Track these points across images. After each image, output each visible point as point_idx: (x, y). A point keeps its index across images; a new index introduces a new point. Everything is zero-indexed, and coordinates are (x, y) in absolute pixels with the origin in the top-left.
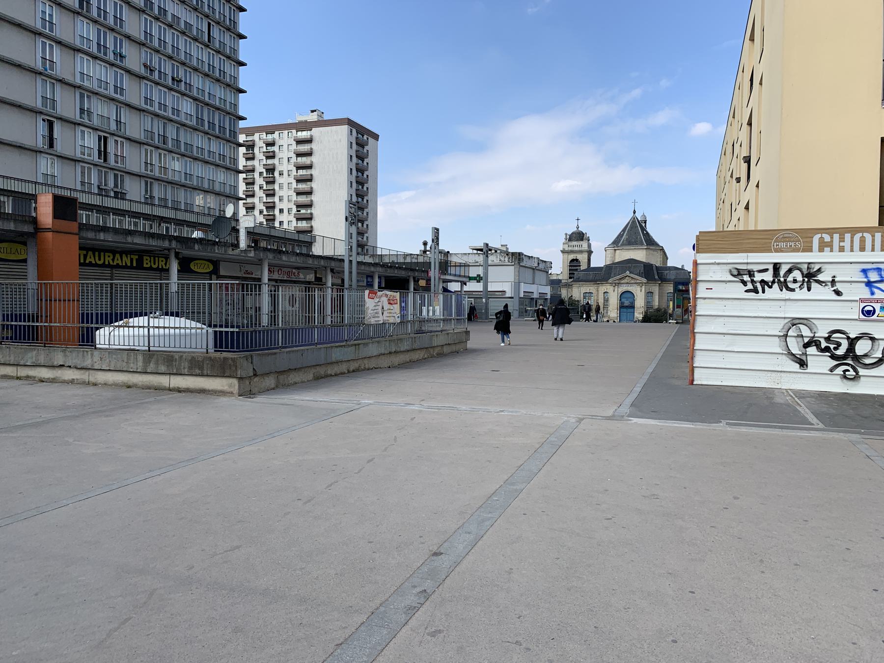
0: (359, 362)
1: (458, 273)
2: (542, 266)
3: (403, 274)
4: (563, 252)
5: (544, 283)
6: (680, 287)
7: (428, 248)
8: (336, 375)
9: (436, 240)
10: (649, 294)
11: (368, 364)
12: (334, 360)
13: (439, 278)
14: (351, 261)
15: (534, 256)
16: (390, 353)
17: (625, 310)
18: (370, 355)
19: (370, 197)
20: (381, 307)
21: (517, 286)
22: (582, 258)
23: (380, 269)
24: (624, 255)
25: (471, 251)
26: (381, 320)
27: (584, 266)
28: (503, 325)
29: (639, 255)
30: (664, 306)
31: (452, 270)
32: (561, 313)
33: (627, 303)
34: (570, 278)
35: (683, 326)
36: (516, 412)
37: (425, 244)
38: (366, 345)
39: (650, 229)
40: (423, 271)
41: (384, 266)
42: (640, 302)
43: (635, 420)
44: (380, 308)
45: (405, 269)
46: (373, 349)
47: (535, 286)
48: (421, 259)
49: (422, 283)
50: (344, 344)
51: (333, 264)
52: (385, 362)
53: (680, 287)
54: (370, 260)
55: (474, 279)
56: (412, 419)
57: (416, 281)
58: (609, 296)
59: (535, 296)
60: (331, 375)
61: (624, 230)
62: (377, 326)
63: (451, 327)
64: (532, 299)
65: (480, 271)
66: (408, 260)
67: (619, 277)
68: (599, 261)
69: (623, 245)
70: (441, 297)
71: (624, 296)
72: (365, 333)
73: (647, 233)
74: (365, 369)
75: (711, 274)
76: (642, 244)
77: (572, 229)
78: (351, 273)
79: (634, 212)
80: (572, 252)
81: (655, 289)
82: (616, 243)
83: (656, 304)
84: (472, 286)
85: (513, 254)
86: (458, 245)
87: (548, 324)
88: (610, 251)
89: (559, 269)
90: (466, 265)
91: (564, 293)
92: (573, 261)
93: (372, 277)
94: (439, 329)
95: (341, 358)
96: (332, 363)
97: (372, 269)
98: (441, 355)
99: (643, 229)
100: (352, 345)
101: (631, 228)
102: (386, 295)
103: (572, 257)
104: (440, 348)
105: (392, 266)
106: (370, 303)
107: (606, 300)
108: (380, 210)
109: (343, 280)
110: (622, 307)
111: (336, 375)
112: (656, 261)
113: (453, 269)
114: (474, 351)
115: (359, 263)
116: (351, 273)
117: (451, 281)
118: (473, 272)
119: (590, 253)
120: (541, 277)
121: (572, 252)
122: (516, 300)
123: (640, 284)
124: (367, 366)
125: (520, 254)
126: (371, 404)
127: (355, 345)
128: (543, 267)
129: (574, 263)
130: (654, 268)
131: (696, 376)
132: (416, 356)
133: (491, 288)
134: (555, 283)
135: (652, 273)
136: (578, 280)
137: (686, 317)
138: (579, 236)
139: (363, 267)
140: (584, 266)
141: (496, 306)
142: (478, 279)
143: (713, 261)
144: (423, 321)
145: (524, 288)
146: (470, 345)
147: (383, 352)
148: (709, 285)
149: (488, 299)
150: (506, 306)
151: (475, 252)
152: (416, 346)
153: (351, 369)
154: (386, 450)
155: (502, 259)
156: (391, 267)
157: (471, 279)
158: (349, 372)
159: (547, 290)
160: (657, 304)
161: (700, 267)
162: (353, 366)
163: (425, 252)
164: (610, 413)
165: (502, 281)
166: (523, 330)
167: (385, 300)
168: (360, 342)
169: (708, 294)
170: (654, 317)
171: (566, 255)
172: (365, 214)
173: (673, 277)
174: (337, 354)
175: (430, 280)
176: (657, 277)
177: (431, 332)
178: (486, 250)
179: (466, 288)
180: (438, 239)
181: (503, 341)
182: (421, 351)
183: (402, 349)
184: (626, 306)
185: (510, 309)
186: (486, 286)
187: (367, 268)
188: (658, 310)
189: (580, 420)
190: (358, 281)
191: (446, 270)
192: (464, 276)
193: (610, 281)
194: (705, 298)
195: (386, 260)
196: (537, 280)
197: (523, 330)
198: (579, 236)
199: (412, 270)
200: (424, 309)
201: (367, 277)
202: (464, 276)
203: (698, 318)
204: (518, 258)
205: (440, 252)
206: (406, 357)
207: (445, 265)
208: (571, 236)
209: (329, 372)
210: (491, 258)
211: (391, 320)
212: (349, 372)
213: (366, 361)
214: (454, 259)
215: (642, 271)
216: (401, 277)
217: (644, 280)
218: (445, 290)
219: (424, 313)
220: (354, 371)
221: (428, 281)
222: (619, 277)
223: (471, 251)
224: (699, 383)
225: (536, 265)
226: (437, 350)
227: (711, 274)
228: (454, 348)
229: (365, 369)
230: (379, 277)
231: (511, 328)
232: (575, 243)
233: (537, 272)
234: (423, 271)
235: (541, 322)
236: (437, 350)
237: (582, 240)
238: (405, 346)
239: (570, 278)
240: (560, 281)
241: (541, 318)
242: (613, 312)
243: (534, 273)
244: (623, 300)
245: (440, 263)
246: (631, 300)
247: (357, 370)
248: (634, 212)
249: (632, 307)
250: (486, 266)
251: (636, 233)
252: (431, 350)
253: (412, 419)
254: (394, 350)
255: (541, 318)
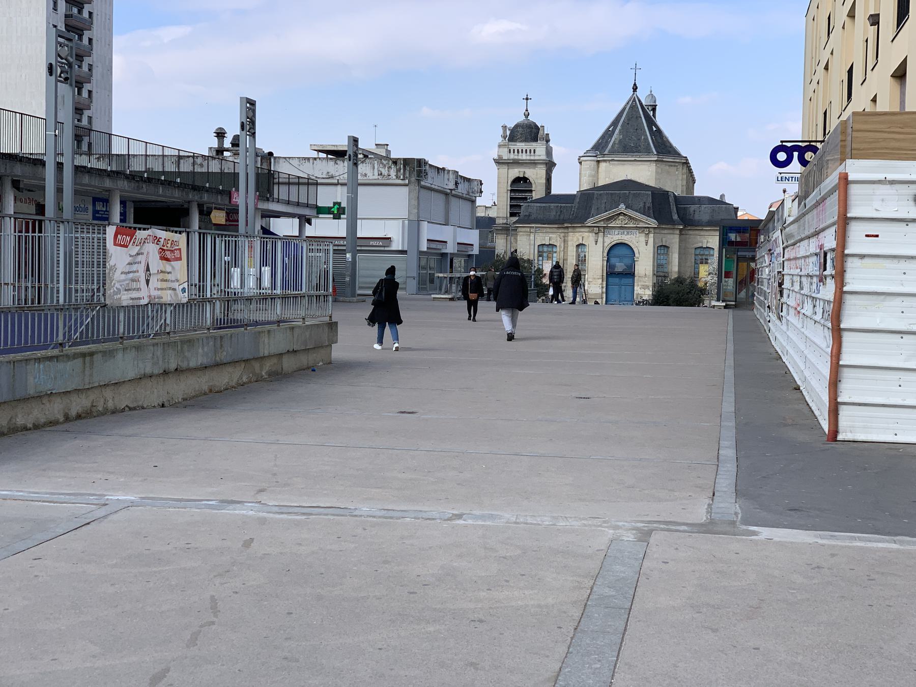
0: (92, 396)
1: (294, 198)
2: (462, 189)
3: (175, 196)
4: (499, 162)
5: (468, 224)
6: (732, 236)
7: (227, 144)
8: (36, 427)
9: (249, 125)
10: (662, 249)
11: (113, 399)
12: (32, 392)
13: (256, 209)
14: (60, 166)
15: (449, 167)
16: (166, 373)
17: (616, 280)
18: (117, 376)
19: (95, 32)
20: (144, 269)
21: (414, 227)
22: (536, 175)
23: (123, 184)
24: (616, 171)
25: (315, 154)
26: (144, 295)
27: (538, 193)
28: (385, 310)
29: (643, 172)
30: (688, 274)
31: (281, 192)
32: (510, 286)
33: (620, 267)
34: (512, 215)
35: (739, 313)
36: (492, 517)
37: (220, 134)
38: (109, 354)
39: (662, 120)
40: (221, 192)
41: (134, 177)
42: (644, 266)
43: (765, 532)
44: (142, 268)
45: (181, 186)
46: (125, 365)
47: (449, 229)
48: (214, 167)
49: (218, 217)
50: (50, 352)
51: (18, 170)
52: (153, 393)
53: (732, 236)
54: (102, 165)
55: (328, 210)
56: (248, 543)
57: (205, 213)
58: (587, 249)
59: (450, 249)
60: (25, 429)
61: (615, 123)
62: (136, 311)
63: (296, 313)
64: (444, 255)
65: (340, 195)
66: (186, 167)
67: (605, 215)
68: (567, 182)
69: (612, 152)
70: (257, 244)
71: (616, 251)
72: (101, 325)
73: (659, 131)
74: (105, 412)
75: (877, 204)
76: (648, 151)
77: (515, 118)
78: (59, 191)
79: (635, 88)
80: (516, 163)
81: (673, 240)
82: (599, 147)
83: (674, 268)
84: (323, 227)
85: (407, 162)
86: (288, 139)
87: (486, 307)
88: (589, 164)
89: (492, 198)
90: (311, 183)
91: (501, 246)
92: (517, 180)
93: (106, 201)
94: (274, 318)
95: (48, 387)
96: (26, 399)
97: (108, 183)
98: (278, 376)
99: (651, 122)
100: (76, 356)
101: (629, 118)
102: (157, 240)
103: (515, 172)
104: (275, 360)
105: (151, 179)
106: (118, 258)
107: (581, 260)
108: (118, 62)
109: (41, 209)
110: (611, 274)
111: (36, 427)
112: (674, 185)
113: (284, 189)
114: (346, 367)
115: (78, 170)
116: (59, 191)
117: (278, 215)
118: (325, 197)
119: (550, 165)
120: (459, 208)
121: (516, 163)
122: (413, 256)
123: (646, 230)
124: (110, 405)
125: (421, 162)
126: (133, 504)
127: (83, 355)
128: (464, 190)
129: (520, 186)
130: (671, 199)
131: (843, 422)
132: (223, 378)
133: (365, 230)
134: (485, 225)
135: (672, 210)
136: (528, 220)
137: (743, 294)
138: (529, 132)
139: (86, 179)
140: (538, 193)
141: (371, 271)
142: (337, 212)
143: (881, 177)
144: (230, 300)
145: (428, 232)
146: (338, 352)
147: (148, 370)
148: (872, 228)
149: (355, 253)
150: (391, 271)
151: (324, 155)
152: (223, 356)
153: (73, 413)
154: (193, 641)
155: (385, 171)
156: (149, 180)
157: (320, 210)
158: (67, 419)
159: (473, 237)
160: (676, 269)
161: (854, 190)
162: (78, 405)
163: (220, 151)
164: (700, 515)
165: (385, 217)
166: (431, 321)
167: (152, 250)
168: (92, 347)
169: (869, 247)
170: (676, 293)
171: (504, 170)
172: (85, 68)
173: (705, 218)
174: (38, 378)
175: (236, 211)
176: (675, 217)
177: (256, 323)
178: (348, 154)
179: (309, 231)
180: (253, 123)
181: (380, 341)
182: (242, 364)
183: (192, 364)
184: (619, 273)
185: (399, 277)
186: (352, 227)
187: (96, 182)
188: (679, 281)
189: (645, 536)
190: (76, 209)
191: (270, 191)
192: (307, 206)
193: (590, 222)
194: (862, 256)
195: (137, 166)
196: (453, 218)
197: (431, 321)
198: (529, 132)
199: (195, 188)
200: (236, 272)
201: (95, 200)
202: (307, 206)
203: (847, 297)
204: (415, 170)
205: (257, 153)
206: (201, 382)
207: (267, 180)
208: (514, 131)
209: (20, 421)
210: (363, 168)
211: (167, 297)
212: (67, 419)
213: (108, 393)
214: (284, 169)
215: (649, 204)
216: (169, 199)
217: (653, 223)
218: (266, 231)
219: (235, 283)
220: (79, 417)
221: (232, 213)
222: (605, 215)
223: (315, 154)
224: (849, 437)
225: (451, 185)
226: (268, 366)
227: (877, 204)
228: (305, 360)
229: (105, 412)
230: (123, 203)
231: (403, 315)
232: (521, 145)
233: (454, 202)
234: (221, 192)
235: (472, 306)
236: (268, 366)
237: (535, 139)
238: (198, 357)
239: (512, 215)
240: (492, 220)
241: (473, 296)
242: (594, 285)
243: (447, 203)
244: (613, 260)
245: (258, 176)
246: (628, 261)
247: (87, 416)
248: (635, 88)
249: (629, 274)
250: (354, 185)
251: (637, 129)
252: (257, 365)
253: (248, 543)
254: (173, 366)
255: (473, 296)
